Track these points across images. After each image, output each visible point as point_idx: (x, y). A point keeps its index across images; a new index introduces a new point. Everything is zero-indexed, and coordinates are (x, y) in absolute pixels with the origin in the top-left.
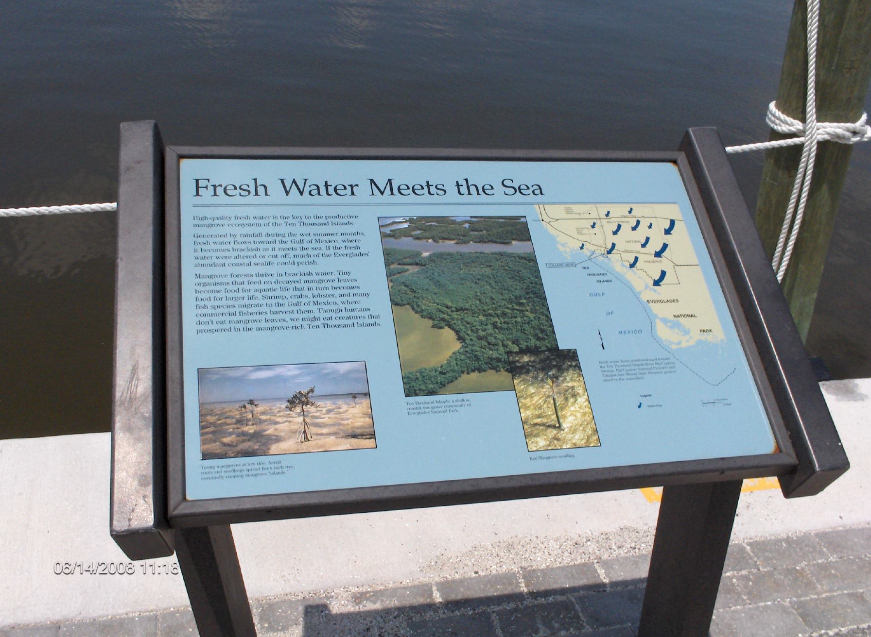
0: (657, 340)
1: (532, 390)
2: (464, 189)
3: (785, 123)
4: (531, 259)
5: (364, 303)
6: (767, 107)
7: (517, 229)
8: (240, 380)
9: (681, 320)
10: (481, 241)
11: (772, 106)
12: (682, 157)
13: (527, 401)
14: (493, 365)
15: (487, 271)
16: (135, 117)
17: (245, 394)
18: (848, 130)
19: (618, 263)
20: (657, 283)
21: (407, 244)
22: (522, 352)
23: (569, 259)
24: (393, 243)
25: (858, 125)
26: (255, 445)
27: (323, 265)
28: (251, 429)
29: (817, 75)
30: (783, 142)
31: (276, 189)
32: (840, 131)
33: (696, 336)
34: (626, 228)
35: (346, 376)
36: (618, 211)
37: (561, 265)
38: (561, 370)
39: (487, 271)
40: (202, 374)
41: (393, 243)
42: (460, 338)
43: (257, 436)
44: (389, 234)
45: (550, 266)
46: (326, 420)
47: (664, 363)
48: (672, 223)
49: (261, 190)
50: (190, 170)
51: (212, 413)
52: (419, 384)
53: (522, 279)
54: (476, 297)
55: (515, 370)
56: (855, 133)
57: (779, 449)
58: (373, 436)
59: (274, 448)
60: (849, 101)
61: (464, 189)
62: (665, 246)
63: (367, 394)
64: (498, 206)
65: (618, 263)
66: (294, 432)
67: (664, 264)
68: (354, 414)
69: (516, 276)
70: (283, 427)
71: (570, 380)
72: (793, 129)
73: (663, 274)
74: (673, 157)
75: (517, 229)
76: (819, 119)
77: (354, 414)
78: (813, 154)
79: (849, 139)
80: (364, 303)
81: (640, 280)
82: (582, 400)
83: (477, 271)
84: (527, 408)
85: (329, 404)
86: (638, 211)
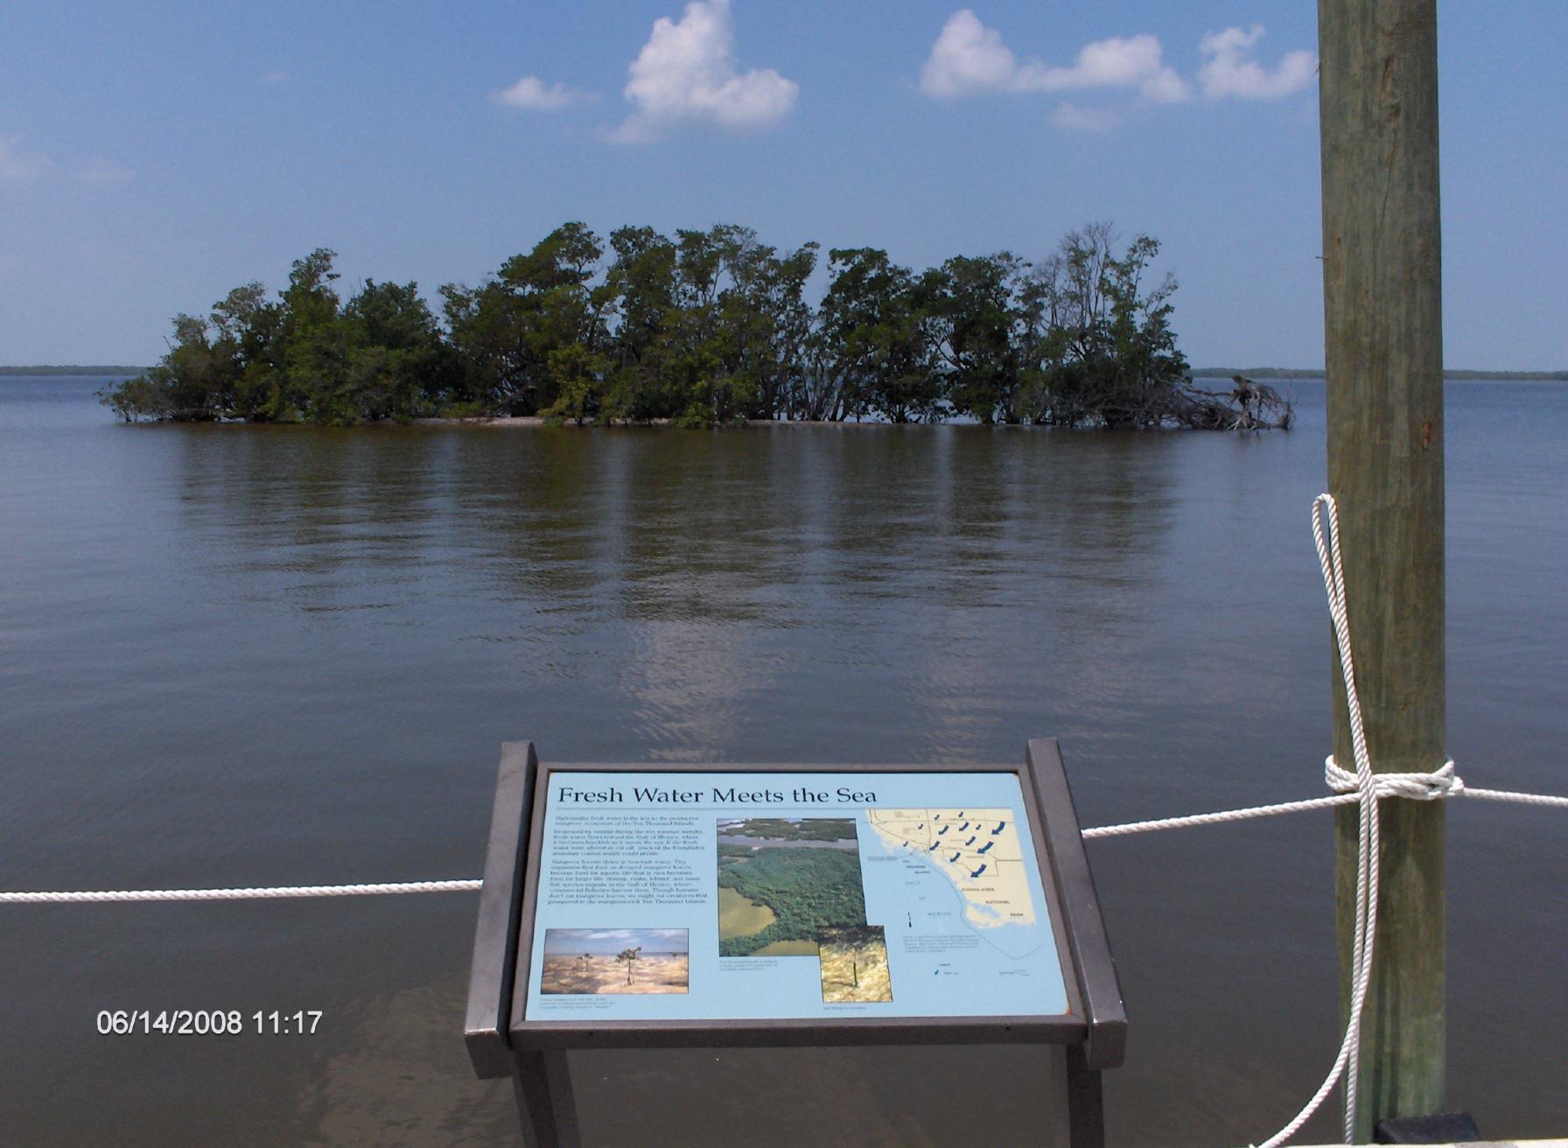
0: (967, 923)
1: (835, 956)
2: (800, 797)
3: (1341, 777)
4: (854, 855)
5: (694, 885)
6: (1324, 766)
7: (846, 829)
8: (581, 939)
9: (994, 906)
10: (809, 838)
11: (1330, 761)
12: (1023, 769)
13: (829, 965)
14: (803, 936)
15: (811, 863)
16: (513, 738)
17: (581, 949)
18: (1421, 782)
19: (939, 859)
20: (975, 875)
21: (741, 840)
22: (831, 926)
23: (891, 853)
24: (727, 840)
25: (1435, 776)
26: (587, 986)
27: (664, 855)
28: (584, 975)
29: (1364, 715)
30: (1339, 799)
31: (629, 797)
32: (1408, 784)
33: (1006, 918)
34: (953, 829)
35: (669, 940)
36: (948, 815)
37: (882, 859)
38: (865, 941)
39: (811, 863)
40: (549, 933)
41: (727, 840)
42: (776, 914)
43: (588, 980)
44: (725, 831)
45: (871, 859)
46: (647, 970)
47: (970, 939)
48: (1002, 825)
49: (616, 797)
50: (557, 781)
51: (554, 961)
52: (730, 948)
53: (842, 870)
54: (797, 882)
55: (821, 940)
56: (1433, 786)
57: (1071, 1012)
58: (686, 984)
59: (601, 989)
60: (1414, 744)
61: (800, 797)
62: (990, 844)
63: (686, 954)
64: (832, 810)
65: (939, 859)
66: (620, 979)
67: (987, 859)
68: (673, 968)
69: (837, 866)
70: (611, 975)
71: (873, 949)
72: (1349, 784)
73: (983, 868)
74: (1014, 767)
75: (846, 829)
76: (1375, 770)
77: (673, 968)
78: (1374, 814)
79: (1424, 794)
80: (694, 885)
81: (959, 874)
82: (881, 966)
83: (801, 862)
84: (827, 969)
85: (652, 959)
86: (968, 815)
